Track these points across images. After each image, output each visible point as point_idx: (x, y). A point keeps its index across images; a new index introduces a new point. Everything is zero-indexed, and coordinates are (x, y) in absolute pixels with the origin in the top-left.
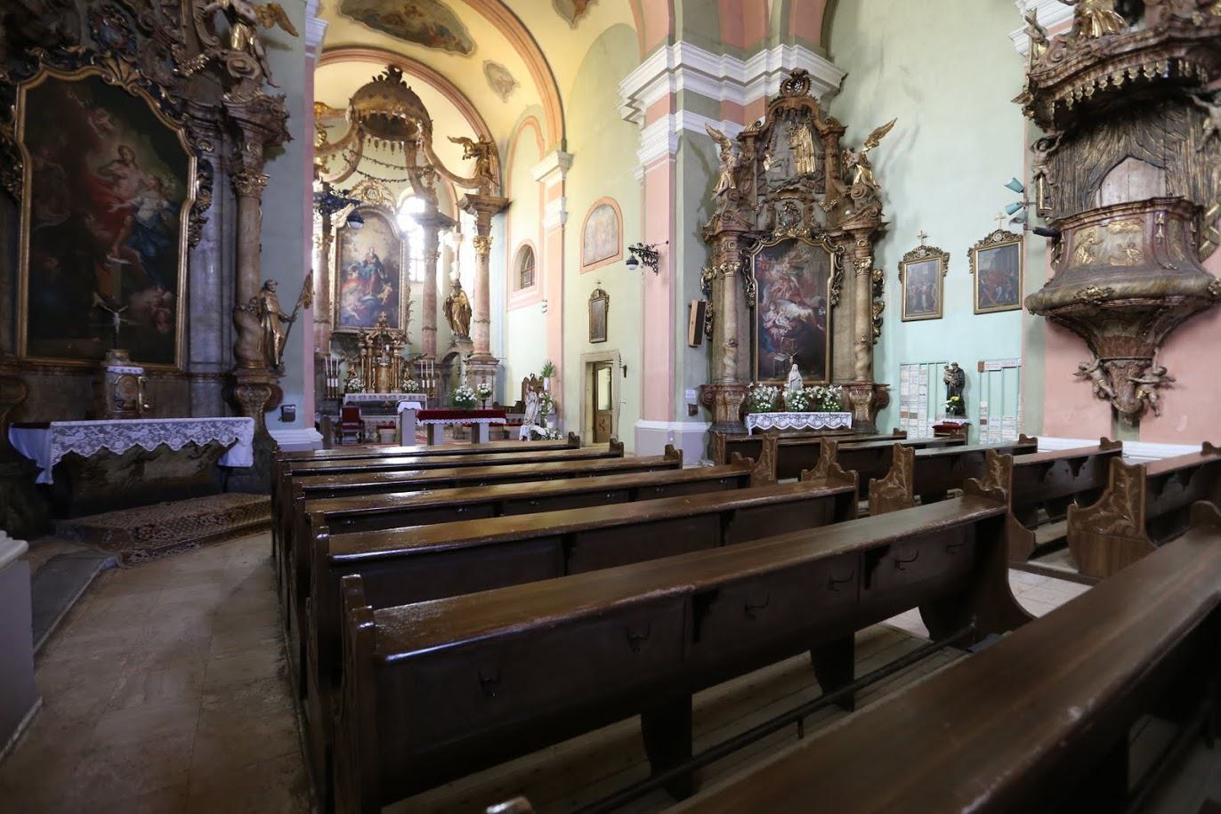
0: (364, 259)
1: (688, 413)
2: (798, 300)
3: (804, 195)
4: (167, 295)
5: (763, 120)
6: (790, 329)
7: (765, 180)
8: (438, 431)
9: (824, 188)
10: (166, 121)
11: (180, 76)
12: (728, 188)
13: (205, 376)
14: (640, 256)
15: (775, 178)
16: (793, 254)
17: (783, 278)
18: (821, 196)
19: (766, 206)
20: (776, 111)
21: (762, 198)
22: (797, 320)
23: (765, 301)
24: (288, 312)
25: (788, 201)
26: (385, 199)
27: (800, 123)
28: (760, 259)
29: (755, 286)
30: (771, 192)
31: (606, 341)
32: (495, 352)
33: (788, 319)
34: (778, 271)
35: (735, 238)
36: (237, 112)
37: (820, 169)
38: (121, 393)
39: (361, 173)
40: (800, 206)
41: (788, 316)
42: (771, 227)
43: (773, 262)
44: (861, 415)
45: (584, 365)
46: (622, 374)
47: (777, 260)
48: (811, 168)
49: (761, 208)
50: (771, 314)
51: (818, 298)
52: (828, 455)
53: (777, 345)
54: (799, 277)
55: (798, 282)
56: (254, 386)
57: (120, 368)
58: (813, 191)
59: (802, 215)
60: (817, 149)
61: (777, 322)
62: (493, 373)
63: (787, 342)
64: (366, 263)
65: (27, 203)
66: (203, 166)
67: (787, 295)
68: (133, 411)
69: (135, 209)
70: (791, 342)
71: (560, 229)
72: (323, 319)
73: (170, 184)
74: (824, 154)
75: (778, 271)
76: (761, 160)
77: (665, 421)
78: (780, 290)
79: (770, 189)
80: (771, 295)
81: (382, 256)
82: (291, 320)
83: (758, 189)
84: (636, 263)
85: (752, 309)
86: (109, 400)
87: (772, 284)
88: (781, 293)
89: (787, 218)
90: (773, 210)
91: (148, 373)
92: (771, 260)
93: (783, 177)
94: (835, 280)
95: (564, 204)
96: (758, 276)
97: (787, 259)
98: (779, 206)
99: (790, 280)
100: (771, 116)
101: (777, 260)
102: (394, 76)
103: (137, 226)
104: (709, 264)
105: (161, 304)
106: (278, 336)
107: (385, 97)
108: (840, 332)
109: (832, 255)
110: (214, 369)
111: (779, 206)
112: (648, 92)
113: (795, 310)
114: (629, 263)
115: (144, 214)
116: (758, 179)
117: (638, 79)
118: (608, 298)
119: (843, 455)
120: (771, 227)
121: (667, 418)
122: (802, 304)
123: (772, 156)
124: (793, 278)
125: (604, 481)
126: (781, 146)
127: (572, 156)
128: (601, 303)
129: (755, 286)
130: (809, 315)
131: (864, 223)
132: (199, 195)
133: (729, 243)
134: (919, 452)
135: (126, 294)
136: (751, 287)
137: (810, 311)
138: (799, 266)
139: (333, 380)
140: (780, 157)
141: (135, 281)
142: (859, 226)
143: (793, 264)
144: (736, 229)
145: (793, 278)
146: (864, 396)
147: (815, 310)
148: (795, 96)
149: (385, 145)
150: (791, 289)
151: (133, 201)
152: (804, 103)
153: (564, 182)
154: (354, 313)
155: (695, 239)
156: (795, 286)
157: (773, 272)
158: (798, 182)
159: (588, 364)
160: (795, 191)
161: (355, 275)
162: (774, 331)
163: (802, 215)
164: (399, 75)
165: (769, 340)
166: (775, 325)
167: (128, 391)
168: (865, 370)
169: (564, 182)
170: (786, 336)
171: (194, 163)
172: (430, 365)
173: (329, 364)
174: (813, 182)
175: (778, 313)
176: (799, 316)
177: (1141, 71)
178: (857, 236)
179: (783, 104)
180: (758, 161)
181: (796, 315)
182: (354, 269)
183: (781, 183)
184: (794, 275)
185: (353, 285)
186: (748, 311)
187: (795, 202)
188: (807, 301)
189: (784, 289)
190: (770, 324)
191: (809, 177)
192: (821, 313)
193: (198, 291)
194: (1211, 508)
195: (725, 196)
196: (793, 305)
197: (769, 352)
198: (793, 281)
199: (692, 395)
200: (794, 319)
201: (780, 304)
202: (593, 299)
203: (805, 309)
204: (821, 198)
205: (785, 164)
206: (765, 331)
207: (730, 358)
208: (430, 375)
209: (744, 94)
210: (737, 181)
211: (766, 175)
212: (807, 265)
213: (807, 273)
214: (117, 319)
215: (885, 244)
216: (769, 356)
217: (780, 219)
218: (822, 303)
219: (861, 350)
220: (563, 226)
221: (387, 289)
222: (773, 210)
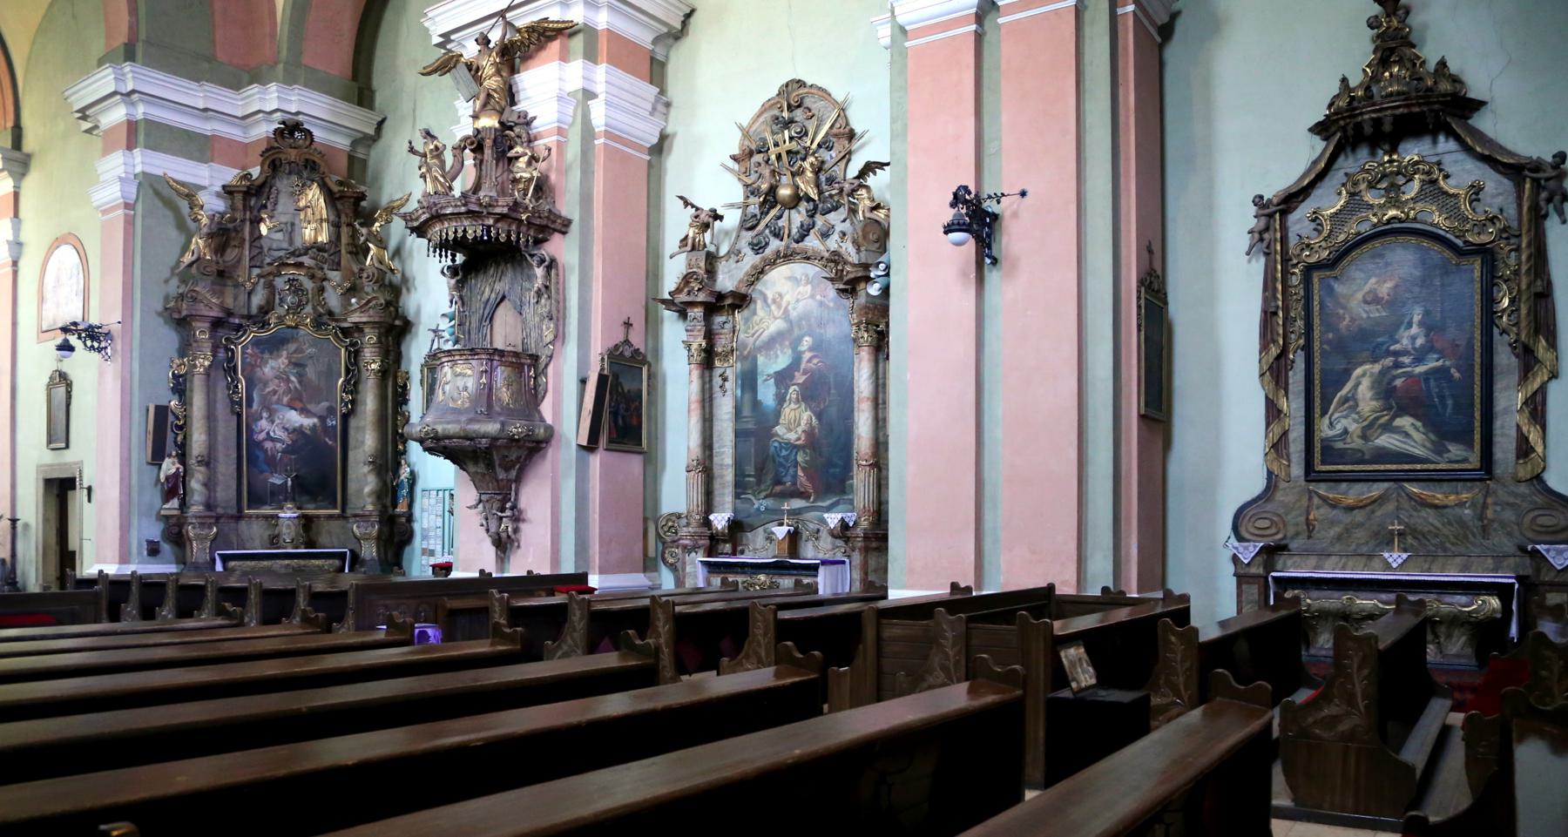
1: (145, 553)
2: (299, 405)
3: (312, 271)
5: (256, 172)
6: (290, 443)
7: (261, 248)
9: (339, 264)
12: (198, 259)
14: (79, 338)
15: (274, 246)
16: (292, 347)
17: (282, 377)
18: (335, 273)
19: (262, 280)
20: (273, 161)
21: (256, 271)
22: (299, 431)
23: (255, 406)
25: (291, 277)
27: (308, 179)
28: (249, 351)
29: (242, 386)
30: (269, 264)
31: (67, 447)
33: (287, 429)
34: (272, 368)
35: (207, 325)
37: (333, 239)
40: (308, 285)
41: (287, 426)
42: (266, 310)
43: (266, 356)
44: (368, 552)
45: (41, 484)
46: (86, 498)
47: (271, 353)
48: (323, 238)
49: (255, 284)
50: (264, 424)
51: (325, 404)
52: (302, 602)
53: (272, 464)
54: (300, 377)
55: (300, 382)
58: (326, 266)
59: (310, 296)
60: (330, 214)
61: (272, 434)
63: (286, 460)
67: (285, 400)
70: (290, 459)
71: (9, 269)
74: (339, 222)
75: (272, 368)
76: (257, 221)
77: (171, 563)
78: (275, 392)
79: (268, 260)
80: (264, 398)
83: (251, 259)
84: (71, 349)
85: (239, 415)
87: (266, 384)
88: (276, 397)
90: (270, 287)
92: (262, 353)
93: (285, 245)
94: (347, 382)
95: (17, 228)
96: (245, 373)
97: (284, 353)
98: (280, 283)
99: (288, 380)
100: (266, 167)
101: (271, 353)
104: (182, 353)
108: (355, 448)
109: (343, 350)
111: (280, 283)
112: (107, 109)
113: (295, 418)
114: (61, 348)
116: (251, 246)
117: (94, 86)
118: (69, 385)
119: (785, 630)
120: (266, 310)
121: (117, 559)
122: (304, 411)
123: (271, 217)
124: (293, 378)
126: (284, 205)
127: (29, 156)
128: (62, 390)
129: (242, 386)
130: (314, 425)
131: (370, 317)
133: (202, 332)
134: (785, 615)
136: (237, 387)
137: (315, 420)
138: (302, 362)
140: (284, 219)
142: (364, 320)
143: (293, 360)
144: (206, 313)
145: (293, 378)
146: (207, 531)
147: (322, 419)
148: (295, 148)
150: (290, 390)
152: (307, 157)
153: (16, 196)
155: (161, 320)
156: (295, 387)
157: (267, 370)
158: (306, 254)
159: (48, 483)
160: (299, 265)
162: (268, 445)
163: (310, 296)
165: (261, 455)
166: (269, 438)
168: (374, 497)
169: (16, 196)
170: (284, 452)
174: (326, 255)
175: (273, 422)
176: (302, 426)
177: (465, 231)
178: (367, 330)
179: (281, 156)
180: (252, 222)
181: (297, 425)
183: (282, 253)
184: (294, 375)
186: (235, 417)
187: (301, 278)
188: (311, 407)
189: (281, 391)
190: (262, 436)
191: (320, 248)
192: (330, 423)
194: (1237, 682)
195: (194, 270)
196: (293, 412)
197: (262, 472)
198: (293, 382)
199: (155, 531)
200: (295, 430)
201: (276, 411)
202: (50, 387)
203: (307, 417)
204: (335, 276)
205: (291, 229)
206: (254, 445)
207: (198, 481)
209: (245, 128)
210: (220, 250)
211: (262, 241)
212: (310, 362)
213: (311, 372)
215: (412, 339)
216: (262, 477)
217: (281, 299)
218: (331, 411)
219: (369, 472)
220: (15, 263)
222: (270, 287)
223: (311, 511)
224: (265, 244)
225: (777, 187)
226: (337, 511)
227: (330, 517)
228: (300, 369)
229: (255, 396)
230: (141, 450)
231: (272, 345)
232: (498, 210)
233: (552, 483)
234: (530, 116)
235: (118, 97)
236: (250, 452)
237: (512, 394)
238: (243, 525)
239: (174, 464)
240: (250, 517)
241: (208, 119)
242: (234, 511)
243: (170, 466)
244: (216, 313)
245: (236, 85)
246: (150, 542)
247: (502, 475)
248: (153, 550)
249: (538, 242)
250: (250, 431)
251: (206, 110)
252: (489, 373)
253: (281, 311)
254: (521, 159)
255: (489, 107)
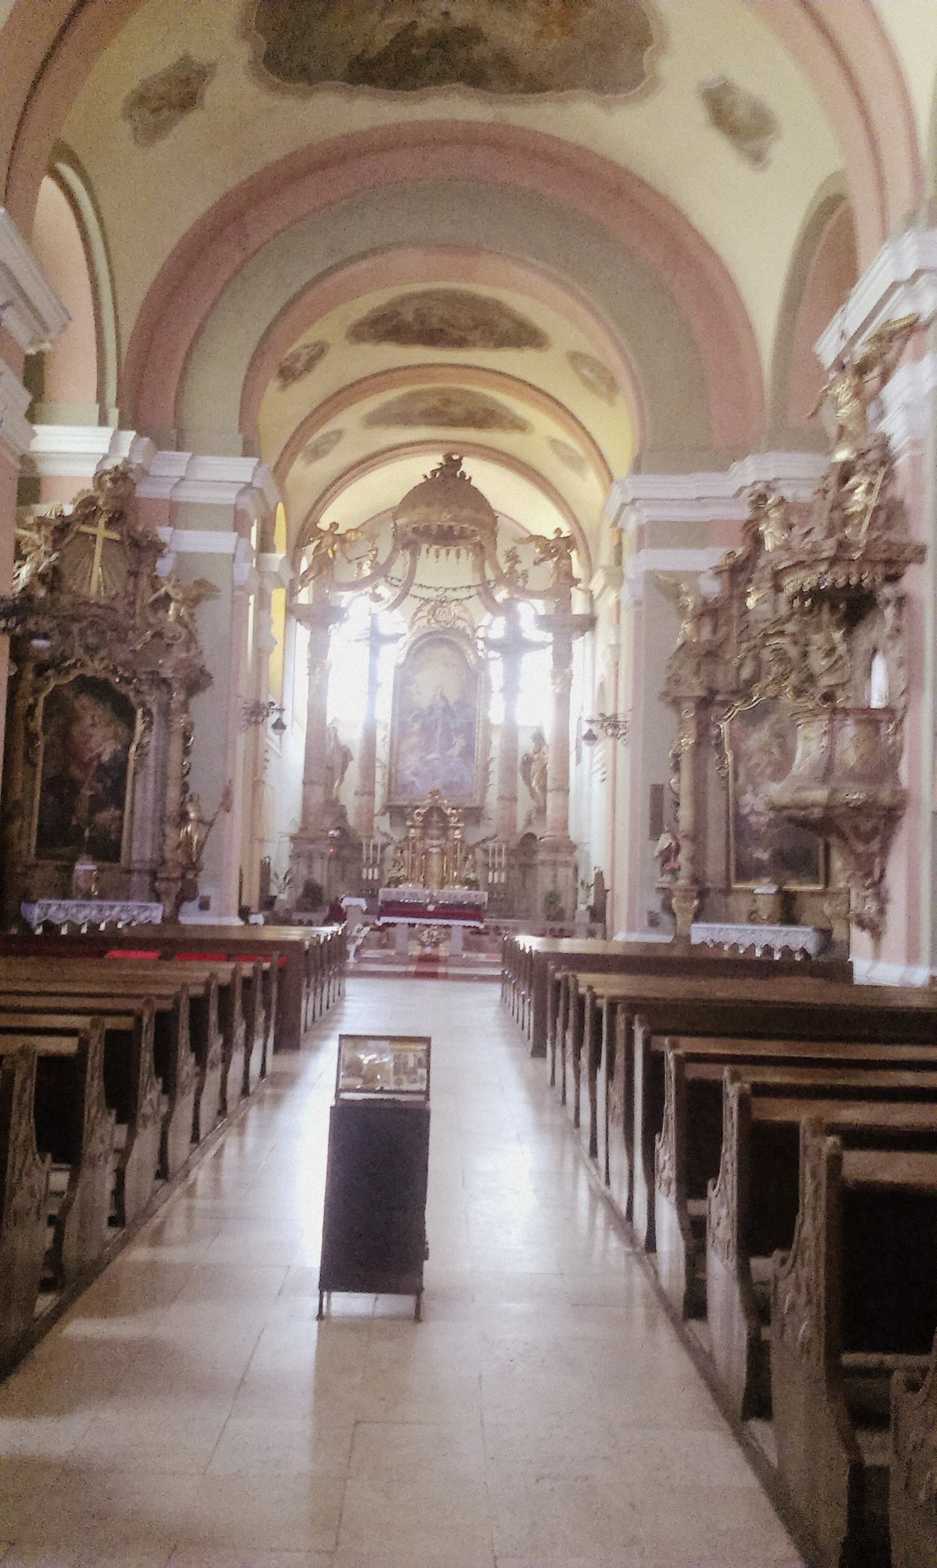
0: (429, 704)
4: (118, 813)
8: (400, 934)
10: (123, 689)
11: (134, 651)
13: (140, 872)
17: (765, 749)
24: (208, 818)
26: (459, 618)
32: (573, 834)
36: (167, 673)
38: (82, 884)
39: (415, 597)
53: (757, 838)
56: (168, 879)
57: (84, 867)
62: (567, 864)
64: (431, 708)
65: (40, 764)
66: (148, 713)
67: (768, 771)
68: (88, 896)
69: (99, 755)
72: (367, 790)
73: (122, 731)
78: (758, 765)
81: (452, 697)
82: (211, 824)
85: (726, 788)
86: (74, 888)
87: (750, 758)
89: (776, 669)
90: (757, 658)
91: (99, 869)
98: (766, 655)
102: (451, 466)
103: (101, 766)
105: (114, 819)
106: (196, 837)
107: (429, 505)
110: (147, 867)
115: (106, 758)
125: (909, 1079)
129: (730, 759)
132: (143, 735)
135: (92, 812)
139: (496, 874)
141: (97, 805)
149: (448, 553)
151: (97, 751)
154: (414, 779)
160: (781, 633)
161: (417, 726)
162: (753, 819)
164: (458, 463)
166: (752, 811)
167: (86, 881)
171: (140, 712)
172: (501, 850)
173: (368, 849)
182: (416, 718)
185: (413, 740)
187: (785, 647)
193: (138, 808)
197: (747, 847)
199: (655, 903)
206: (739, 819)
208: (500, 864)
214: (87, 833)
221: (459, 742)
222: (757, 658)
223: (793, 886)
224: (751, 618)
225: (482, 552)
226: (819, 888)
227: (812, 894)
228: (781, 740)
229: (742, 771)
230: (645, 829)
231: (754, 717)
232: (825, 555)
233: (909, 859)
234: (887, 435)
235: (627, 508)
236: (739, 828)
237: (861, 756)
238: (731, 899)
239: (667, 839)
240: (738, 891)
241: (705, 506)
242: (722, 885)
243: (665, 841)
244: (699, 692)
245: (723, 468)
246: (650, 913)
247: (860, 848)
248: (654, 922)
249: (893, 578)
250: (736, 803)
251: (699, 499)
252: (831, 733)
253: (765, 681)
254: (856, 491)
255: (844, 438)
